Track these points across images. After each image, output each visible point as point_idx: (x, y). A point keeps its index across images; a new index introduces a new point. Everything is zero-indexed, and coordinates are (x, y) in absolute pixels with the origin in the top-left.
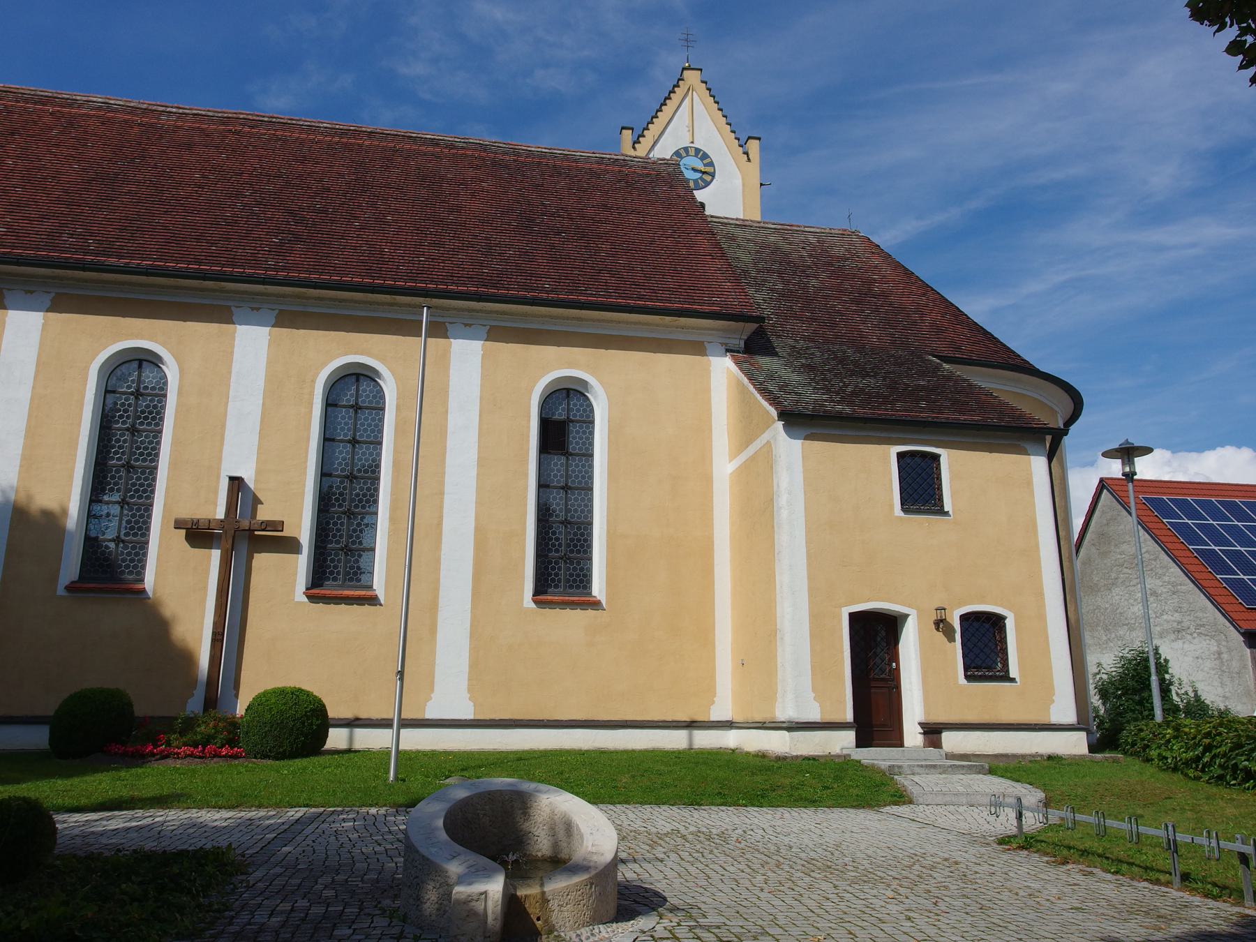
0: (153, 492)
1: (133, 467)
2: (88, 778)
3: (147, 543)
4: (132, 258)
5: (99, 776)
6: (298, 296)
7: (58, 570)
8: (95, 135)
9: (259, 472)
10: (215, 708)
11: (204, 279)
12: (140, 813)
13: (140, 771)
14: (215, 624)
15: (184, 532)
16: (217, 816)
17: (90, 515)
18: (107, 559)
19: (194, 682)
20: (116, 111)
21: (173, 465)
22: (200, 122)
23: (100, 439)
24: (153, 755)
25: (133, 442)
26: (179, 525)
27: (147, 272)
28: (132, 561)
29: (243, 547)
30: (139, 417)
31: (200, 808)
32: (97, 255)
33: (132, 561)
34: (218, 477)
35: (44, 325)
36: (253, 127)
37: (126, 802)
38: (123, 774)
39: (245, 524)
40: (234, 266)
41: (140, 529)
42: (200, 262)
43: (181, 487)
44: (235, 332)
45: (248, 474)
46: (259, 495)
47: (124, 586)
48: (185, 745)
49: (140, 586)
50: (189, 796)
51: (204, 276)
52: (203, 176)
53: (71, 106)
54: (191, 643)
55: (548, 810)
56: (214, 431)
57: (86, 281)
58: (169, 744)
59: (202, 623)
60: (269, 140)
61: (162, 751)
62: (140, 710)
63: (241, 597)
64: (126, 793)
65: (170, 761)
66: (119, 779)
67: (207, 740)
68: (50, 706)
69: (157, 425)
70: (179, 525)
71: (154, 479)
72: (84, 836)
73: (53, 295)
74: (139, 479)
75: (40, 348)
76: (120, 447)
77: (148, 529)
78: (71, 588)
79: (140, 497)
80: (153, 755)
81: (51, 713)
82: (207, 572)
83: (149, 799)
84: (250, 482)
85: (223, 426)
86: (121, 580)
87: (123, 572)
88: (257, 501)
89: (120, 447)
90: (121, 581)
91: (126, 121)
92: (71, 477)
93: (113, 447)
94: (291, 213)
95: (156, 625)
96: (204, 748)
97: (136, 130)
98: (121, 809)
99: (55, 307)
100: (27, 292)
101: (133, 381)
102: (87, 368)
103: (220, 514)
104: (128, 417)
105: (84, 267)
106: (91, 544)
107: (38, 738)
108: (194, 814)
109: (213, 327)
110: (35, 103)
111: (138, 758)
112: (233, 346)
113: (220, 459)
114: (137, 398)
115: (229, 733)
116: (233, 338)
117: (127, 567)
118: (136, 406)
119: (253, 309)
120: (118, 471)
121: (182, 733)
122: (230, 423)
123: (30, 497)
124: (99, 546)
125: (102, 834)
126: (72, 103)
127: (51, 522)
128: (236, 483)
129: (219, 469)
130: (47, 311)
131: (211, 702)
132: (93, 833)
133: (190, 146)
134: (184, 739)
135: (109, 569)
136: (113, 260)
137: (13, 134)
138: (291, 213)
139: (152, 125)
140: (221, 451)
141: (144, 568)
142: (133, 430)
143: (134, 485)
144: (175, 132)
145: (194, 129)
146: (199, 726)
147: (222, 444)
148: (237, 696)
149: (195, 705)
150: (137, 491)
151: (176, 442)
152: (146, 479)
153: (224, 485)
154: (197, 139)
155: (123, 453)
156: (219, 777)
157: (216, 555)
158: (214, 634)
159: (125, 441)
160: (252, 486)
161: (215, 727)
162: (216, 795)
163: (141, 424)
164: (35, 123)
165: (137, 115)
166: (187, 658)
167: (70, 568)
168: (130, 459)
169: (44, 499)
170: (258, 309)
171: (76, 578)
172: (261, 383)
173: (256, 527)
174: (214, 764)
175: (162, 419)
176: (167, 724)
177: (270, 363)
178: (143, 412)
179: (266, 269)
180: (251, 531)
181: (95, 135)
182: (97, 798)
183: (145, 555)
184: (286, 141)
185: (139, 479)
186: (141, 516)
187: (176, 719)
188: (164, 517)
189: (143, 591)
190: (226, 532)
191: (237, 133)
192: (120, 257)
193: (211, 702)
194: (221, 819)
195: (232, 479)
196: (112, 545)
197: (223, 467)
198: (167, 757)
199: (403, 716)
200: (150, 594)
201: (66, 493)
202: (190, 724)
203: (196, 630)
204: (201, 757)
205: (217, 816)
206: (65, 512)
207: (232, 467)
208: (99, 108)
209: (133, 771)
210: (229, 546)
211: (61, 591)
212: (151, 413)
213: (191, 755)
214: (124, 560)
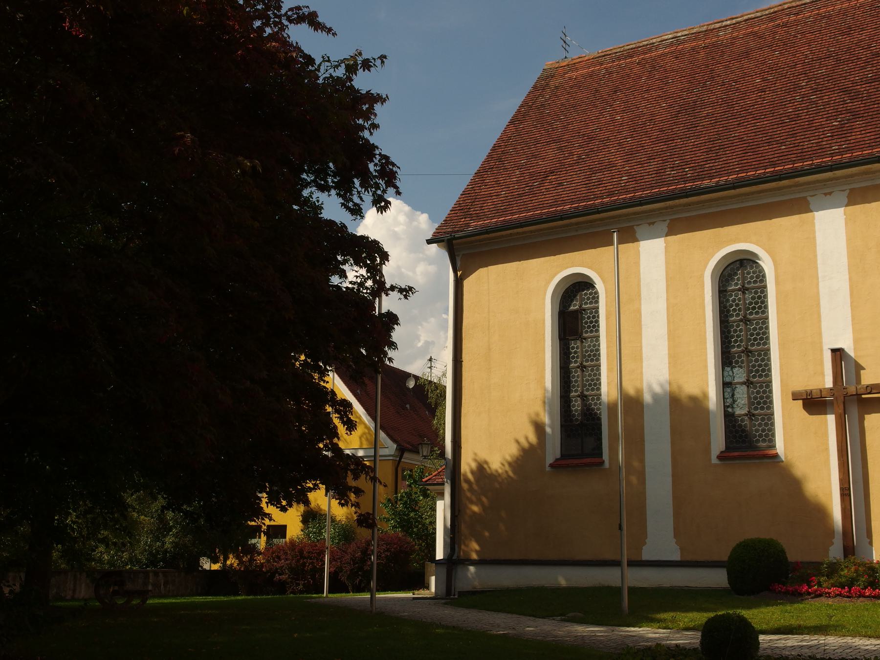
0: (770, 370)
1: (751, 352)
2: (764, 610)
3: (773, 414)
4: (720, 176)
5: (770, 609)
6: (866, 173)
7: (710, 443)
8: (673, 71)
9: (856, 341)
10: (854, 555)
11: (780, 179)
12: (807, 637)
13: (801, 606)
14: (841, 481)
15: (801, 402)
16: (868, 642)
17: (726, 385)
18: (744, 431)
19: (829, 532)
20: (684, 41)
21: (782, 346)
22: (752, 26)
23: (722, 332)
24: (809, 594)
25: (748, 330)
26: (796, 396)
27: (734, 186)
28: (763, 430)
29: (854, 410)
30: (748, 309)
31: (854, 636)
32: (694, 180)
33: (763, 430)
34: (822, 350)
35: (666, 247)
36: (797, 14)
37: (795, 628)
38: (788, 608)
39: (852, 390)
40: (803, 160)
41: (765, 403)
42: (774, 165)
43: (793, 366)
44: (814, 218)
45: (846, 344)
46: (862, 362)
47: (761, 453)
48: (833, 585)
49: (773, 452)
50: (843, 627)
51: (779, 177)
52: (764, 80)
53: (650, 50)
54: (822, 498)
55: (507, 468)
56: (810, 309)
57: (689, 204)
58: (819, 584)
59: (830, 480)
60: (814, 22)
61: (816, 591)
62: (793, 556)
63: (860, 463)
64: (794, 622)
65: (823, 599)
66: (786, 611)
67: (851, 583)
68: (724, 555)
69: (763, 312)
70: (796, 396)
71: (769, 359)
72: (772, 649)
73: (668, 221)
74: (756, 361)
75: (666, 268)
76: (738, 336)
77: (771, 402)
78: (721, 457)
79: (761, 376)
80: (809, 594)
81: (725, 558)
82: (826, 434)
83: (811, 627)
84: (851, 352)
85: (818, 305)
86: (757, 447)
87: (758, 441)
88: (859, 368)
89: (738, 336)
90: (757, 448)
91: (693, 49)
92: (706, 367)
93: (733, 337)
94: (845, 91)
95: (793, 485)
96: (848, 589)
97: (702, 54)
98: (793, 634)
99: (672, 231)
100: (650, 224)
101: (738, 279)
102: (702, 276)
103: (829, 383)
104: (740, 310)
105: (686, 194)
106: (730, 418)
107: (719, 578)
108: (849, 640)
109: (795, 219)
110: (625, 58)
111: (796, 596)
112: (814, 232)
113: (820, 334)
114: (744, 293)
115: (870, 576)
116: (813, 224)
117: (760, 436)
118: (745, 299)
119: (826, 194)
120: (740, 357)
121: (829, 576)
122: (824, 302)
123: (680, 387)
124: (736, 421)
125: (785, 648)
126: (651, 48)
127: (697, 404)
128: (838, 354)
129: (821, 343)
130: (667, 235)
131: (849, 550)
132: (777, 647)
133: (747, 54)
134: (832, 581)
135: (748, 438)
136: (706, 183)
137: (616, 92)
138: (845, 91)
139: (714, 45)
140: (820, 327)
141: (773, 435)
142: (746, 321)
143: (754, 366)
144: (732, 43)
145: (748, 35)
146: (842, 570)
147: (820, 321)
148: (871, 543)
149: (835, 552)
150: (757, 371)
151: (780, 326)
152: (763, 360)
153: (828, 357)
154: (752, 44)
155: (741, 341)
156: (866, 613)
157: (831, 419)
158: (842, 489)
159: (741, 331)
160: (852, 354)
161: (856, 571)
162: (865, 627)
163: (751, 314)
164: (628, 76)
165: (700, 39)
166: (820, 513)
167: (718, 441)
168: (747, 345)
169: (690, 388)
170: (830, 194)
171: (724, 449)
172: (845, 260)
173: (862, 391)
174: (860, 602)
175: (766, 307)
176: (815, 568)
177: (849, 240)
178: (751, 303)
179: (832, 155)
180: (858, 395)
181: (673, 71)
182: (774, 624)
183: (773, 424)
184: (829, 17)
185: (756, 361)
186: (764, 392)
187: (822, 564)
188: (782, 391)
189: (776, 456)
190: (836, 398)
191: (785, 25)
192: (711, 177)
193: (849, 550)
194: (871, 644)
195: (834, 351)
196: (747, 422)
197: (824, 340)
198: (820, 595)
199: (370, 531)
200: (783, 458)
201: (705, 381)
202: (833, 569)
203: (825, 485)
204: (848, 597)
205: (868, 642)
206: (705, 396)
207: (831, 341)
208: (671, 44)
209: (796, 605)
210: (841, 411)
211: (714, 460)
212: (756, 303)
213: (840, 595)
214: (757, 431)
